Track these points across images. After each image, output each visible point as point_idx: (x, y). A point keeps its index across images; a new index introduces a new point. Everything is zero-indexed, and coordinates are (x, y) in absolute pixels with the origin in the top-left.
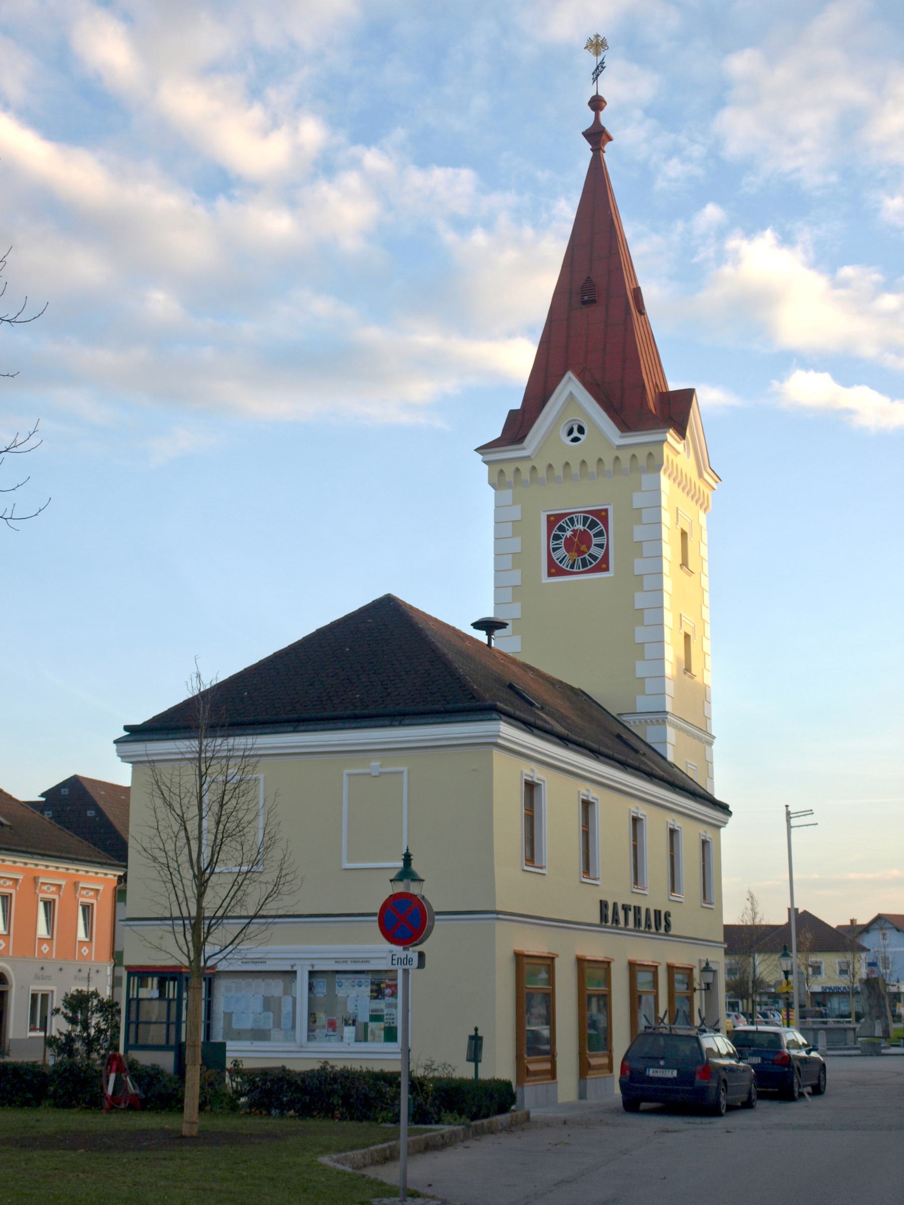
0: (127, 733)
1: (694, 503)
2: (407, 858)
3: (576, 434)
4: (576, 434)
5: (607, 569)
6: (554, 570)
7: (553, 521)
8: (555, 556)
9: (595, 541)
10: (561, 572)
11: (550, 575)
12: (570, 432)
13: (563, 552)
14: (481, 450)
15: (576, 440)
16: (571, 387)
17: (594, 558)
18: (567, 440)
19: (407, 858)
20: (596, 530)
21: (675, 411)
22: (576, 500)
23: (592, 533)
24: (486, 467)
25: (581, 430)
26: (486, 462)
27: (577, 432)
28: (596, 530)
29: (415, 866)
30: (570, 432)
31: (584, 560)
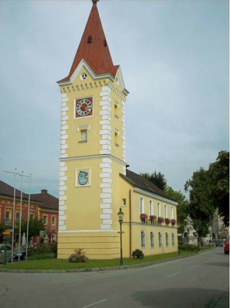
0: (224, 217)
1: (81, 90)
2: (120, 209)
3: (84, 77)
4: (84, 77)
5: (92, 114)
6: (78, 115)
7: (78, 101)
8: (78, 112)
9: (88, 107)
10: (79, 116)
11: (76, 117)
12: (83, 76)
13: (80, 110)
14: (58, 82)
15: (84, 78)
16: (82, 63)
17: (88, 112)
18: (82, 78)
19: (120, 209)
20: (89, 104)
21: (112, 70)
22: (84, 94)
23: (88, 105)
24: (59, 87)
25: (86, 76)
26: (60, 86)
27: (85, 76)
28: (89, 104)
29: (122, 211)
30: (83, 76)
31: (85, 113)
